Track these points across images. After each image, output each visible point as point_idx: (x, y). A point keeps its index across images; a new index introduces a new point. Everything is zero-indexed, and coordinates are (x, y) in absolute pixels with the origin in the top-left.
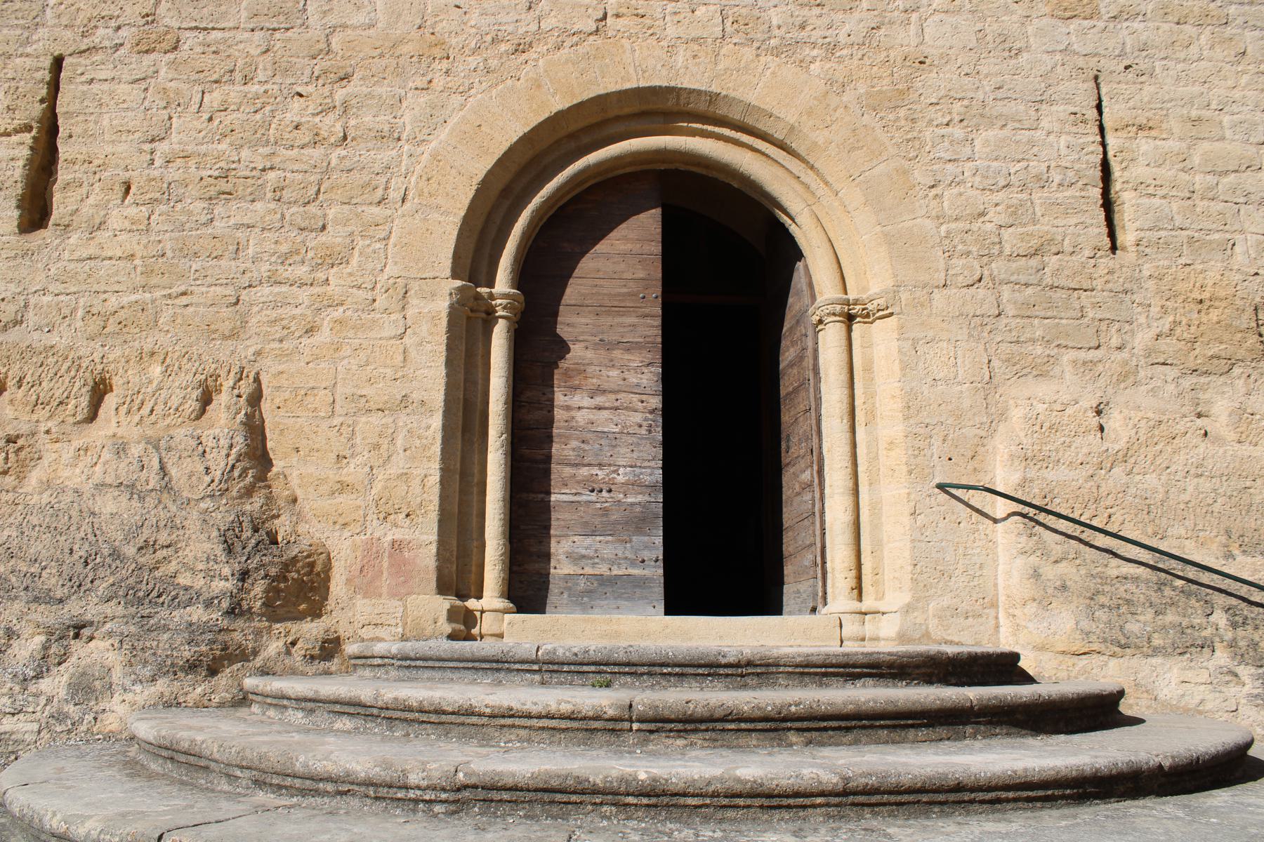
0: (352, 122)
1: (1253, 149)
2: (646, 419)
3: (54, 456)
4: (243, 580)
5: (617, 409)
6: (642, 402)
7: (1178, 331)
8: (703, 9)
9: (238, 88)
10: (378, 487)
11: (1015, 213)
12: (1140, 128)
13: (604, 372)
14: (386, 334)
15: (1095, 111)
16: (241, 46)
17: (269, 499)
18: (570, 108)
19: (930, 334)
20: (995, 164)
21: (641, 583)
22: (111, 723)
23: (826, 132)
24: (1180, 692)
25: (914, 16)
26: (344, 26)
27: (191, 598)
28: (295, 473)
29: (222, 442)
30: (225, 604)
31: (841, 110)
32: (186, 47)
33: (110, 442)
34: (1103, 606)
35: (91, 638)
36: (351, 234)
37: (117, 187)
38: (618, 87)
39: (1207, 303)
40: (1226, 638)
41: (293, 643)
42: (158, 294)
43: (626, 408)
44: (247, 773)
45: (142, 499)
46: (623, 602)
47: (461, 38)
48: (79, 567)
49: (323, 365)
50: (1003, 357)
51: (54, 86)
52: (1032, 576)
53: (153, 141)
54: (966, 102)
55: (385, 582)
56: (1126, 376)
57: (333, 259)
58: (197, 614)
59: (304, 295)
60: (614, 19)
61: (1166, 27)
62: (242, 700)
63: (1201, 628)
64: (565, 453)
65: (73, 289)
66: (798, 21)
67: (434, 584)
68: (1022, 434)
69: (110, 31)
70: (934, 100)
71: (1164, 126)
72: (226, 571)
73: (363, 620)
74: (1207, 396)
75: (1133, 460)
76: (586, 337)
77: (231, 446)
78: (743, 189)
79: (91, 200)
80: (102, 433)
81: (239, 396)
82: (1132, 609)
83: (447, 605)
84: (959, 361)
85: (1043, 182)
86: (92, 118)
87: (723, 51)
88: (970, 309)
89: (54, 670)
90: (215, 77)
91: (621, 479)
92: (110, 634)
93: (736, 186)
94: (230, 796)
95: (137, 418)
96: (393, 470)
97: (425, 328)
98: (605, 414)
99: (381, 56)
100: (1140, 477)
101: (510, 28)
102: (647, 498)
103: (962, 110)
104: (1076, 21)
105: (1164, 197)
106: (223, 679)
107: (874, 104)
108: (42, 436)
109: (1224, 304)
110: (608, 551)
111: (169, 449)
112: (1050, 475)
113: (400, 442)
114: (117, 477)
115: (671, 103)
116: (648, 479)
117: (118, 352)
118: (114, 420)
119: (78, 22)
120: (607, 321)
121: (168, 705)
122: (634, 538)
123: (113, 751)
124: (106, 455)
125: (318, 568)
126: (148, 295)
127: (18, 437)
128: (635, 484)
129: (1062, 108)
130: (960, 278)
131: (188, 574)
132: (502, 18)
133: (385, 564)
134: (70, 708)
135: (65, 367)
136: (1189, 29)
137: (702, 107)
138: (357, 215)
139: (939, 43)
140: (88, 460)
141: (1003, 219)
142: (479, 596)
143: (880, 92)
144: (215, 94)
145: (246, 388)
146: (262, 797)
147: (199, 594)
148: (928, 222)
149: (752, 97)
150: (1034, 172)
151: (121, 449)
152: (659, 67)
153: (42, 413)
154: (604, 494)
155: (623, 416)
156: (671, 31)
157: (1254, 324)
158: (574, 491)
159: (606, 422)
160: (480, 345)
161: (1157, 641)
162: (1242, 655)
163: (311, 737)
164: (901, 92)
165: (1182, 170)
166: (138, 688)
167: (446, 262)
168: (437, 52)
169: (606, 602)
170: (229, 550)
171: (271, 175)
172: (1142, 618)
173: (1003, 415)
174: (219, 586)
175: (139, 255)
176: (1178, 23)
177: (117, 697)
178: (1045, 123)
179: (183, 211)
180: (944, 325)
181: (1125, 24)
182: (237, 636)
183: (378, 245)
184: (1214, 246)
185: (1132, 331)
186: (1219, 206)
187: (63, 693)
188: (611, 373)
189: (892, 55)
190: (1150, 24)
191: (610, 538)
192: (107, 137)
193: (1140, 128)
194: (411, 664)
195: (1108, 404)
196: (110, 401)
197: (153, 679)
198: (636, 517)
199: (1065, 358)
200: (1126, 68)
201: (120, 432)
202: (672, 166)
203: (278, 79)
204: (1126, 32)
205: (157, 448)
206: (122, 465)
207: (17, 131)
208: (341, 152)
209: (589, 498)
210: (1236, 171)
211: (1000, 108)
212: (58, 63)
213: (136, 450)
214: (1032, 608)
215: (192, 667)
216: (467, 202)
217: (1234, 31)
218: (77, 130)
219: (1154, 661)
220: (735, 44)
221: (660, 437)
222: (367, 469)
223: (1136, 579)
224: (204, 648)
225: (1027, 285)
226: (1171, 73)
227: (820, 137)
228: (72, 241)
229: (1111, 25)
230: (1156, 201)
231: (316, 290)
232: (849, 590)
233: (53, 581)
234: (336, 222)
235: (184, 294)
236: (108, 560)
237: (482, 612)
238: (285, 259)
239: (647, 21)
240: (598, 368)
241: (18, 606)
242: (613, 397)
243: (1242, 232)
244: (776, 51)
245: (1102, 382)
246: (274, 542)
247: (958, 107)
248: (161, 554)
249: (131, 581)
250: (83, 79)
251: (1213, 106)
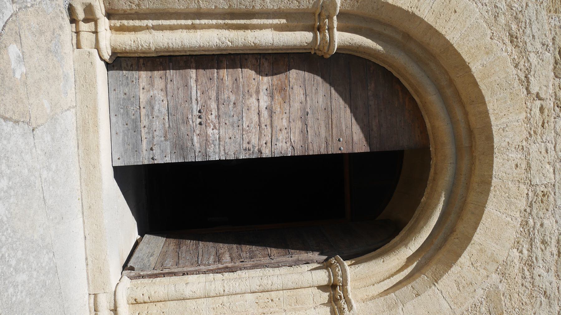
2: (254, 147)
6: (266, 143)
13: (285, 116)
18: (473, 76)
21: (136, 150)
23: (468, 263)
31: (485, 273)
38: (491, 111)
43: (260, 132)
46: (121, 137)
60: (539, 106)
64: (226, 92)
66: (547, 239)
76: (309, 102)
78: (420, 205)
91: (210, 131)
93: (422, 200)
98: (256, 118)
102: (198, 150)
110: (157, 124)
116: (210, 150)
120: (322, 116)
122: (168, 143)
128: (206, 141)
143: (500, 300)
152: (507, 140)
154: (199, 120)
155: (255, 130)
158: (199, 99)
160: (295, 24)
169: (121, 125)
188: (284, 120)
191: (167, 125)
198: (183, 143)
202: (433, 155)
209: (195, 110)
220: (527, 194)
221: (241, 157)
232: (134, 297)
239: (539, 130)
240: (287, 111)
242: (268, 123)
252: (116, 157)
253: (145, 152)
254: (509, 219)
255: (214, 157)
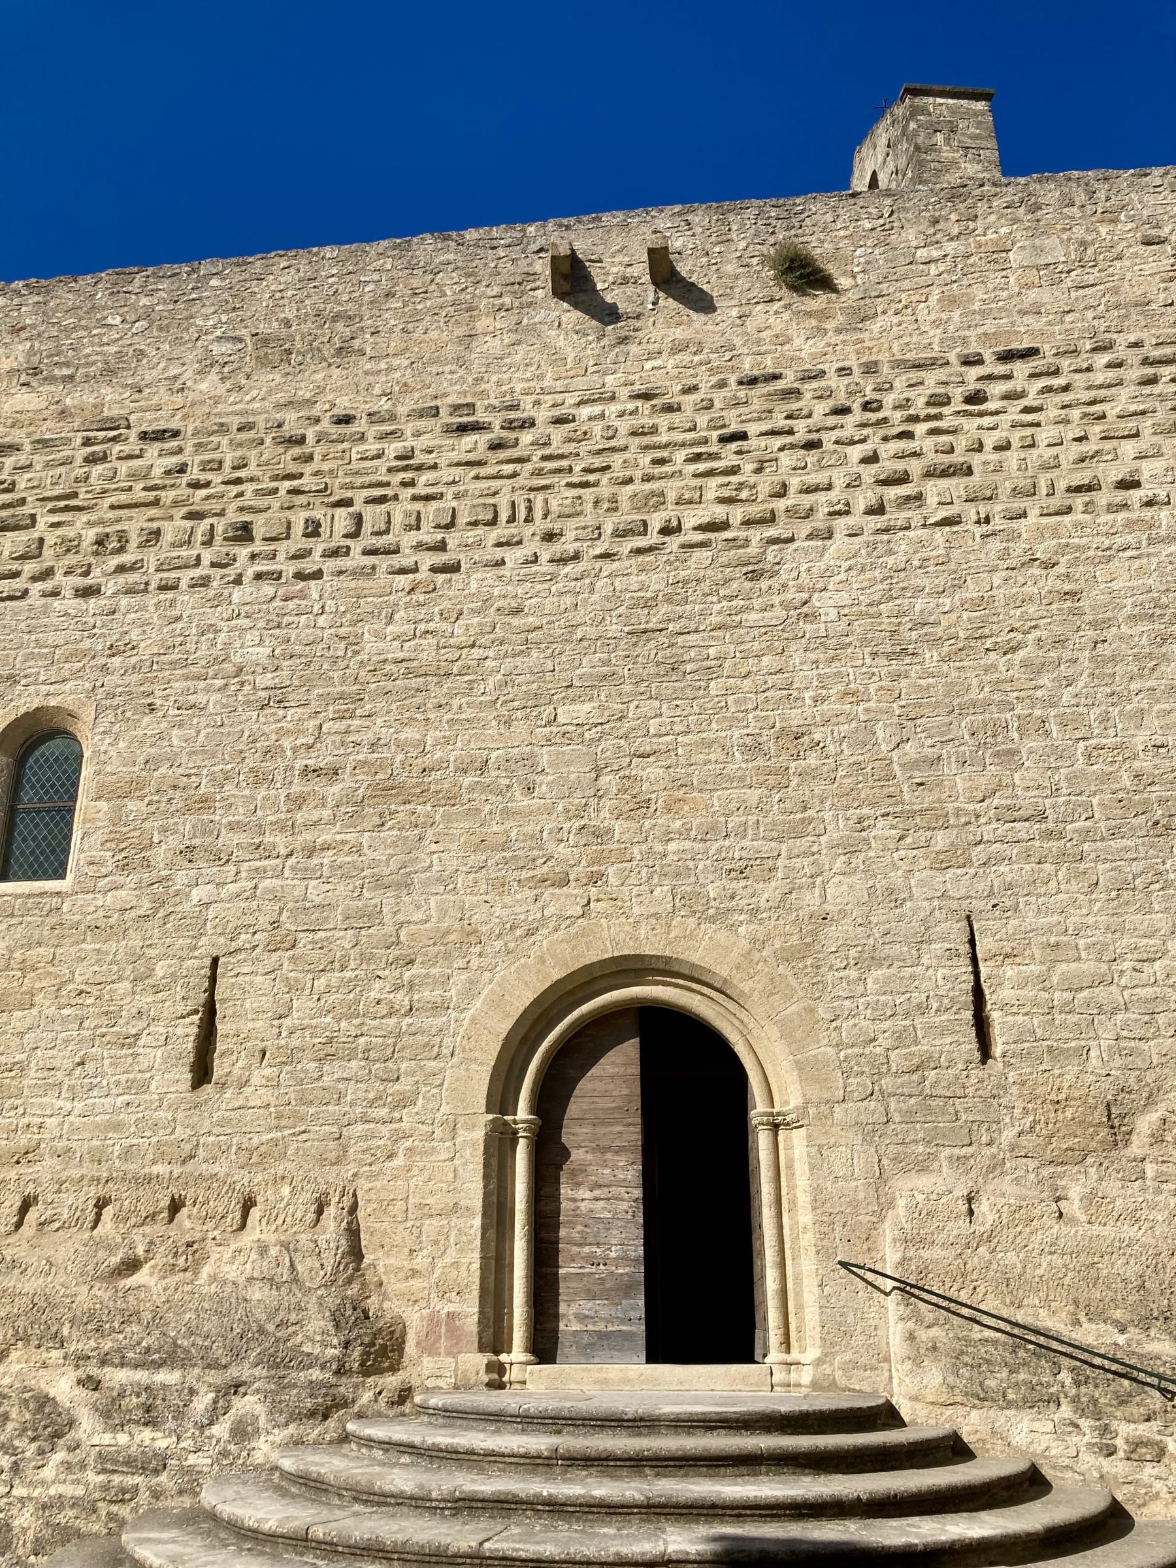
0: (416, 997)
1: (1105, 966)
2: (631, 1207)
3: (218, 1256)
4: (346, 1348)
5: (609, 1199)
7: (1038, 1127)
8: (659, 889)
9: (337, 974)
10: (438, 1272)
11: (900, 1037)
12: (1007, 956)
14: (442, 1157)
15: (967, 945)
16: (338, 942)
17: (364, 1285)
19: (833, 1141)
20: (884, 998)
21: (628, 1336)
22: (258, 1458)
23: (750, 982)
24: (1029, 1440)
25: (819, 879)
26: (408, 922)
27: (309, 1361)
28: (381, 1264)
29: (332, 1245)
30: (334, 1367)
31: (761, 964)
32: (301, 945)
33: (256, 1245)
34: (966, 1365)
35: (245, 1394)
36: (417, 1082)
37: (256, 1054)
38: (600, 958)
39: (1064, 1103)
40: (1070, 1394)
41: (380, 1393)
42: (287, 1132)
43: (616, 1199)
44: (349, 1493)
45: (278, 1289)
47: (489, 927)
48: (237, 1341)
49: (399, 1182)
50: (891, 1156)
51: (213, 979)
52: (908, 1339)
53: (280, 1018)
54: (860, 949)
55: (443, 1344)
56: (995, 1168)
57: (404, 1102)
58: (316, 1374)
59: (385, 1130)
61: (1028, 867)
62: (345, 1438)
63: (1049, 1385)
65: (229, 1131)
67: (476, 1345)
68: (904, 1221)
69: (249, 936)
70: (834, 949)
71: (1027, 953)
72: (335, 1341)
73: (427, 1373)
74: (1063, 1183)
75: (996, 1240)
77: (338, 1248)
79: (240, 1064)
80: (250, 1238)
81: (343, 1209)
82: (992, 1368)
83: (485, 1361)
84: (855, 1162)
85: (922, 1009)
86: (239, 1002)
87: (674, 923)
88: (863, 1119)
89: (221, 1418)
90: (321, 967)
91: (613, 1255)
92: (258, 1391)
94: (341, 1507)
95: (274, 1227)
96: (448, 1260)
97: (468, 1152)
98: (602, 1203)
99: (435, 944)
100: (1002, 1254)
101: (522, 917)
102: (632, 1269)
103: (856, 955)
104: (951, 870)
105: (1027, 1014)
106: (331, 1423)
107: (788, 956)
108: (209, 1242)
109: (1078, 1103)
111: (296, 1251)
112: (926, 1254)
113: (452, 1239)
114: (262, 1272)
115: (639, 965)
117: (260, 1177)
118: (258, 1229)
119: (228, 931)
120: (601, 1130)
121: (296, 1443)
123: (262, 1479)
124: (254, 1256)
125: (397, 1335)
126: (279, 1134)
127: (194, 1242)
128: (624, 1259)
129: (939, 946)
130: (856, 1094)
131: (310, 1344)
132: (518, 909)
133: (443, 1330)
134: (232, 1447)
135: (224, 1190)
136: (1048, 867)
137: (661, 966)
138: (421, 1068)
139: (839, 900)
140: (242, 1259)
141: (888, 1043)
142: (509, 1352)
143: (792, 946)
144: (322, 980)
145: (347, 1202)
146: (357, 1507)
147: (317, 1358)
148: (830, 1049)
149: (695, 958)
150: (915, 1002)
151: (263, 1250)
153: (210, 1225)
154: (602, 1267)
156: (636, 910)
157: (1105, 1119)
159: (602, 1210)
161: (1011, 1396)
162: (1083, 1410)
163: (386, 1469)
164: (808, 945)
165: (1043, 990)
166: (276, 1431)
167: (483, 1102)
168: (473, 939)
170: (337, 1326)
171: (362, 1040)
172: (998, 1375)
173: (891, 1204)
174: (330, 1352)
175: (273, 1104)
176: (1039, 863)
177: (262, 1439)
178: (925, 960)
179: (302, 1070)
180: (843, 1133)
181: (993, 869)
182: (342, 1389)
183: (435, 1091)
184: (1071, 1052)
185: (999, 1130)
186: (1075, 1018)
187: (227, 1436)
189: (801, 913)
190: (1015, 867)
192: (249, 1016)
193: (1007, 956)
194: (452, 1415)
195: (978, 1192)
196: (255, 1213)
197: (286, 1424)
199: (943, 1155)
200: (994, 906)
201: (263, 1237)
203: (364, 966)
204: (994, 876)
205: (288, 1249)
206: (265, 1263)
207: (189, 1015)
208: (408, 1020)
210: (1090, 987)
211: (887, 950)
212: (215, 961)
213: (274, 1251)
214: (908, 1365)
215: (312, 1414)
216: (495, 1055)
217: (1087, 865)
218: (229, 1012)
219: (1008, 1412)
221: (641, 1221)
222: (430, 1259)
223: (995, 1342)
224: (320, 1400)
225: (910, 1096)
226: (1033, 907)
227: (746, 986)
228: (227, 1095)
229: (981, 871)
230: (1020, 1018)
231: (394, 1126)
233: (220, 1351)
234: (406, 1073)
235: (304, 1132)
236: (256, 1335)
237: (511, 1364)
238: (371, 1103)
241: (197, 1371)
242: (606, 1190)
243: (1097, 1038)
244: (713, 920)
245: (973, 1174)
246: (367, 1317)
247: (853, 953)
248: (291, 1329)
249: (272, 1350)
250: (232, 973)
251: (1070, 932)
252: (636, 1360)
253: (632, 1328)
254: (707, 938)
255: (641, 1251)
